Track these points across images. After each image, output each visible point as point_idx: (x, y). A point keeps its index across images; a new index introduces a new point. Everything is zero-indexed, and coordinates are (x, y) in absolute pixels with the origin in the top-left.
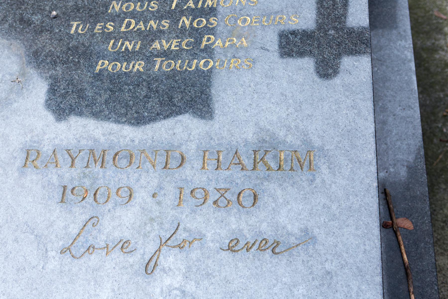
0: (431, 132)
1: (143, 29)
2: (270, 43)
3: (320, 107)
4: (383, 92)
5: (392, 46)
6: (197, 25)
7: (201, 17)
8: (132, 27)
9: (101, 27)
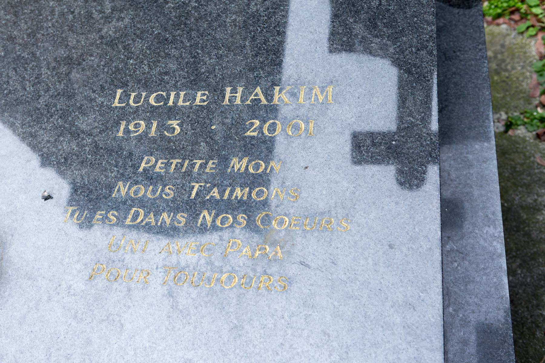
0: (532, 322)
1: (153, 223)
2: (312, 256)
3: (373, 355)
4: (465, 297)
5: (476, 234)
6: (221, 224)
7: (227, 213)
8: (139, 220)
9: (101, 217)
